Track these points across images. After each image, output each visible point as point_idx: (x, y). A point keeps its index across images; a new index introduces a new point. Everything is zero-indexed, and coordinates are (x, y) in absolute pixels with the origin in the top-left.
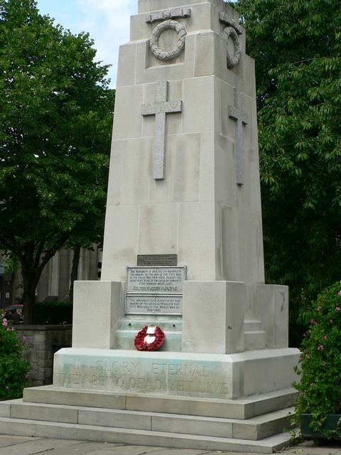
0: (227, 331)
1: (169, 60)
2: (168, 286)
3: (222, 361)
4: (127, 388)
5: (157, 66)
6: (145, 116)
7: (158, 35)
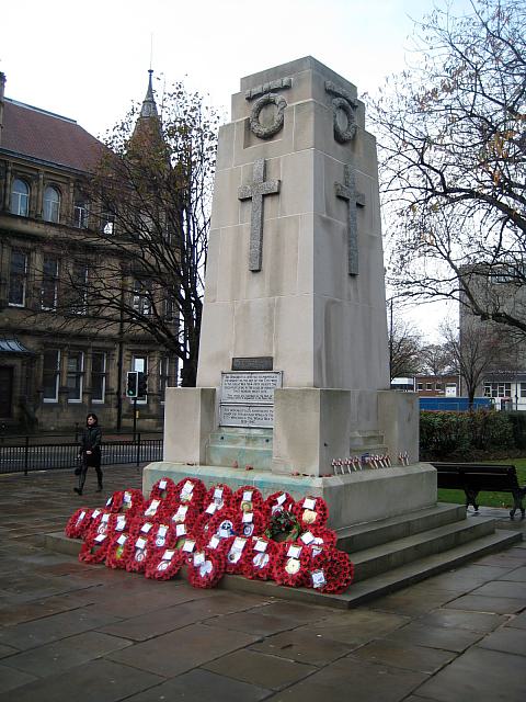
0: (321, 449)
1: (269, 136)
2: (264, 394)
3: (311, 485)
4: (71, 537)
5: (258, 144)
6: (243, 200)
7: (258, 111)
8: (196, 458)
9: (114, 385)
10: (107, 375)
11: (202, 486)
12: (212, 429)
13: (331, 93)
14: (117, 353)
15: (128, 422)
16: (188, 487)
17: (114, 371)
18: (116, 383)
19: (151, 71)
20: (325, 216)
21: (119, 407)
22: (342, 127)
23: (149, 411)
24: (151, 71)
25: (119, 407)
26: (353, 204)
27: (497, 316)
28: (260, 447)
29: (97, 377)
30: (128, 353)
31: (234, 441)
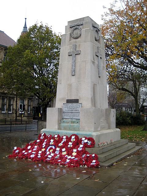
1: (77, 38)
2: (76, 109)
5: (73, 40)
8: (57, 127)
9: (15, 107)
10: (13, 105)
11: (78, 137)
12: (61, 120)
13: (94, 27)
14: (16, 98)
15: (19, 118)
16: (73, 137)
17: (15, 103)
18: (15, 107)
19: (26, 19)
20: (93, 60)
21: (16, 114)
22: (96, 36)
23: (25, 115)
24: (26, 19)
25: (16, 114)
26: (99, 58)
27: (123, 89)
28: (75, 125)
29: (10, 105)
30: (19, 99)
31: (68, 123)
